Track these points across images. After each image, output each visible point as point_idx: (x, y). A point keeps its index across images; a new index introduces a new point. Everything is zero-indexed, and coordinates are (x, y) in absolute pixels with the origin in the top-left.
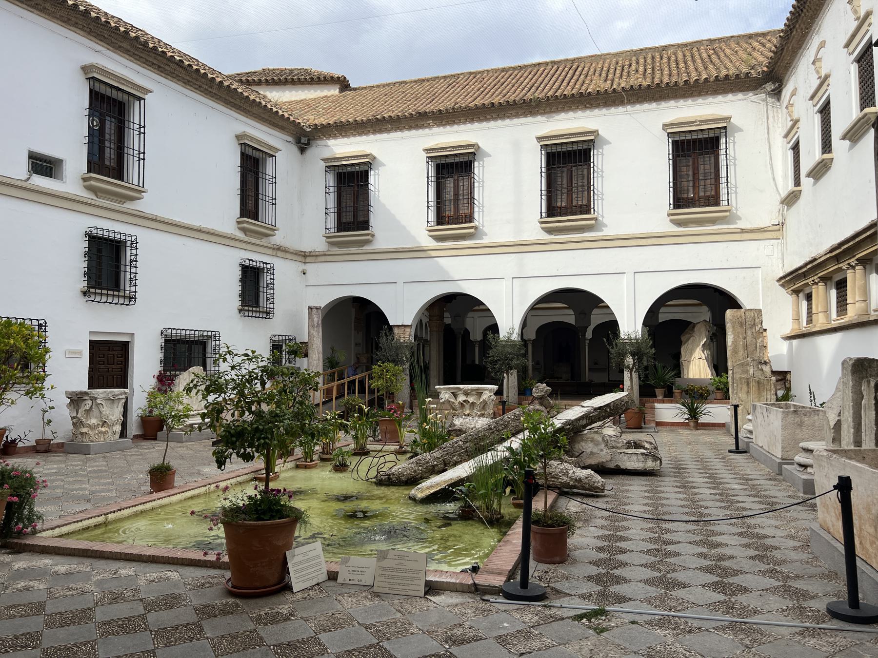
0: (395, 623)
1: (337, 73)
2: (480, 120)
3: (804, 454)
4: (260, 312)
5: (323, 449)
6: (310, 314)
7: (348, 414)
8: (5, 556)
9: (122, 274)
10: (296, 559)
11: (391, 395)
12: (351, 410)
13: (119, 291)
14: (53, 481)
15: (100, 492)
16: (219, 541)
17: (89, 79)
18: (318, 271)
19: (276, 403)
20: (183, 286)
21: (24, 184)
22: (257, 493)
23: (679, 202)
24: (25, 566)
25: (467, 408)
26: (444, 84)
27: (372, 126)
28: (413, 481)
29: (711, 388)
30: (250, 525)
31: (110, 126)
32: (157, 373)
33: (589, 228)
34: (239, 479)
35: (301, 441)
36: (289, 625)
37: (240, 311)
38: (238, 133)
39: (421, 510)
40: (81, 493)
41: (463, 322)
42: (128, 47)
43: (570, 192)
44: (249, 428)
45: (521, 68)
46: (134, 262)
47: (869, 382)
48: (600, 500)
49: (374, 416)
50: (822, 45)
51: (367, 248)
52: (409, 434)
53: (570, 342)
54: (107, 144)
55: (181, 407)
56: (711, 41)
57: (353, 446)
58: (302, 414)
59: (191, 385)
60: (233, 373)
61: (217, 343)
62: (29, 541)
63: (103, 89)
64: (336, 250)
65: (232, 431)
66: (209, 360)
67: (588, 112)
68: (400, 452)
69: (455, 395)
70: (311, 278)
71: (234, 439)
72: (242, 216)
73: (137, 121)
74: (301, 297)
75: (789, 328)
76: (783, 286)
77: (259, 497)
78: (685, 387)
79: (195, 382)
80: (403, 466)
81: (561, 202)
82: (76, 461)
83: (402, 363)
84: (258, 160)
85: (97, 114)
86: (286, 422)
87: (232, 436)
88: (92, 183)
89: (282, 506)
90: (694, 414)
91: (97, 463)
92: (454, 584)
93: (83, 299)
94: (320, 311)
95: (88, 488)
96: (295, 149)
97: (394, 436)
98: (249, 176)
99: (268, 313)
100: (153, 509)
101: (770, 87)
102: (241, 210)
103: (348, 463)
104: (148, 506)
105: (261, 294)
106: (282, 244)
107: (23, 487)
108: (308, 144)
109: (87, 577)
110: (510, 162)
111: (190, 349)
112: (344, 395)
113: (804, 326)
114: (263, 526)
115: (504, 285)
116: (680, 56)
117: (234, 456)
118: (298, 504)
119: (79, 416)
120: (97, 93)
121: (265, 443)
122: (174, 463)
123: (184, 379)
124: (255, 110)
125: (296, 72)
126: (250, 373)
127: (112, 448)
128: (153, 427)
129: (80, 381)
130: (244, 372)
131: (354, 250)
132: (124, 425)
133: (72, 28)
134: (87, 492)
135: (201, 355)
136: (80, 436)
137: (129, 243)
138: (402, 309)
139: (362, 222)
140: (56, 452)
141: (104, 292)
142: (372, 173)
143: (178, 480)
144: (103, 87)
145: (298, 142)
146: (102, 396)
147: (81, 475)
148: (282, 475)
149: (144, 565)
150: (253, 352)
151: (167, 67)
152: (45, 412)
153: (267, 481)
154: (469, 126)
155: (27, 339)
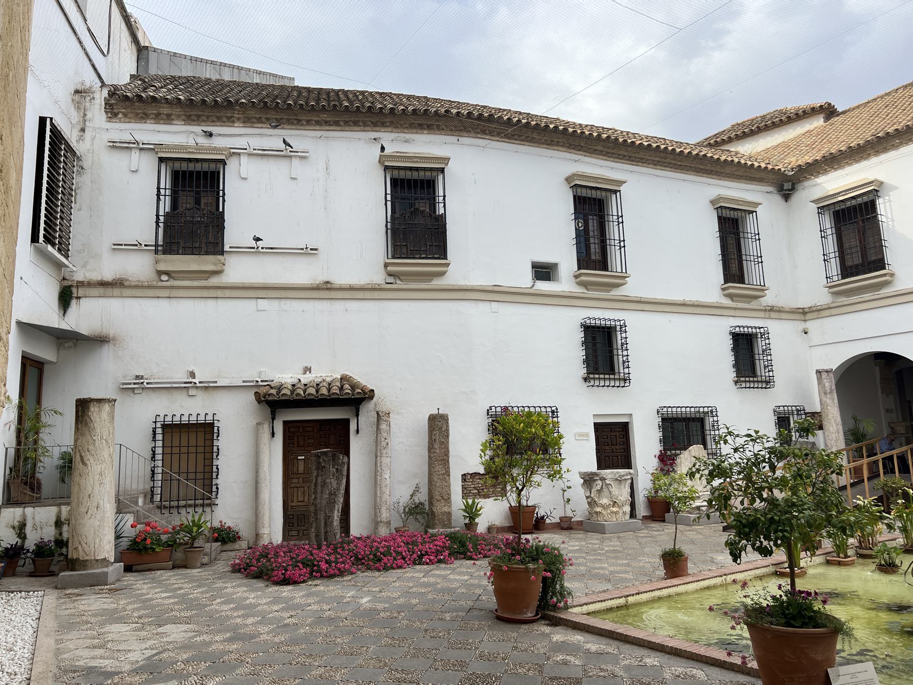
1: (818, 102)
4: (758, 382)
5: (860, 542)
6: (819, 379)
7: (888, 499)
8: (545, 627)
9: (615, 357)
12: (892, 494)
13: (614, 374)
14: (577, 558)
15: (618, 572)
16: (745, 642)
19: (790, 489)
20: (677, 362)
22: (782, 593)
24: (561, 640)
27: (872, 148)
30: (779, 631)
31: (593, 224)
32: (658, 453)
34: (758, 572)
35: (828, 532)
37: (736, 382)
38: (713, 197)
40: (602, 572)
42: (602, 149)
44: (763, 519)
51: (885, 291)
54: (592, 240)
55: (685, 489)
57: (901, 541)
58: (826, 502)
59: (694, 470)
60: (737, 455)
61: (715, 419)
64: (843, 300)
65: (744, 521)
66: (708, 437)
71: (747, 530)
72: (726, 281)
73: (615, 213)
77: (784, 598)
79: (697, 466)
82: (594, 539)
84: (737, 220)
85: (581, 216)
86: (807, 512)
87: (745, 526)
89: (814, 612)
91: (612, 543)
93: (585, 385)
94: (831, 375)
95: (607, 567)
96: (777, 199)
98: (729, 239)
99: (767, 382)
100: (669, 596)
102: (725, 275)
103: (898, 562)
104: (665, 592)
105: (757, 362)
106: (774, 304)
107: (554, 563)
108: (793, 189)
109: (615, 660)
111: (687, 427)
112: (879, 475)
117: (749, 548)
118: (836, 610)
120: (580, 197)
121: (784, 536)
122: (685, 548)
123: (686, 460)
124: (728, 170)
125: (769, 117)
126: (755, 455)
127: (622, 528)
128: (660, 509)
129: (590, 464)
130: (749, 454)
131: (867, 296)
132: (633, 505)
134: (607, 572)
135: (699, 433)
137: (618, 328)
139: (874, 262)
140: (576, 529)
141: (602, 376)
143: (691, 567)
144: (584, 190)
146: (610, 476)
147: (600, 554)
148: (811, 571)
149: (667, 656)
150: (757, 432)
151: (636, 155)
152: (564, 491)
153: (792, 576)
155: (544, 427)
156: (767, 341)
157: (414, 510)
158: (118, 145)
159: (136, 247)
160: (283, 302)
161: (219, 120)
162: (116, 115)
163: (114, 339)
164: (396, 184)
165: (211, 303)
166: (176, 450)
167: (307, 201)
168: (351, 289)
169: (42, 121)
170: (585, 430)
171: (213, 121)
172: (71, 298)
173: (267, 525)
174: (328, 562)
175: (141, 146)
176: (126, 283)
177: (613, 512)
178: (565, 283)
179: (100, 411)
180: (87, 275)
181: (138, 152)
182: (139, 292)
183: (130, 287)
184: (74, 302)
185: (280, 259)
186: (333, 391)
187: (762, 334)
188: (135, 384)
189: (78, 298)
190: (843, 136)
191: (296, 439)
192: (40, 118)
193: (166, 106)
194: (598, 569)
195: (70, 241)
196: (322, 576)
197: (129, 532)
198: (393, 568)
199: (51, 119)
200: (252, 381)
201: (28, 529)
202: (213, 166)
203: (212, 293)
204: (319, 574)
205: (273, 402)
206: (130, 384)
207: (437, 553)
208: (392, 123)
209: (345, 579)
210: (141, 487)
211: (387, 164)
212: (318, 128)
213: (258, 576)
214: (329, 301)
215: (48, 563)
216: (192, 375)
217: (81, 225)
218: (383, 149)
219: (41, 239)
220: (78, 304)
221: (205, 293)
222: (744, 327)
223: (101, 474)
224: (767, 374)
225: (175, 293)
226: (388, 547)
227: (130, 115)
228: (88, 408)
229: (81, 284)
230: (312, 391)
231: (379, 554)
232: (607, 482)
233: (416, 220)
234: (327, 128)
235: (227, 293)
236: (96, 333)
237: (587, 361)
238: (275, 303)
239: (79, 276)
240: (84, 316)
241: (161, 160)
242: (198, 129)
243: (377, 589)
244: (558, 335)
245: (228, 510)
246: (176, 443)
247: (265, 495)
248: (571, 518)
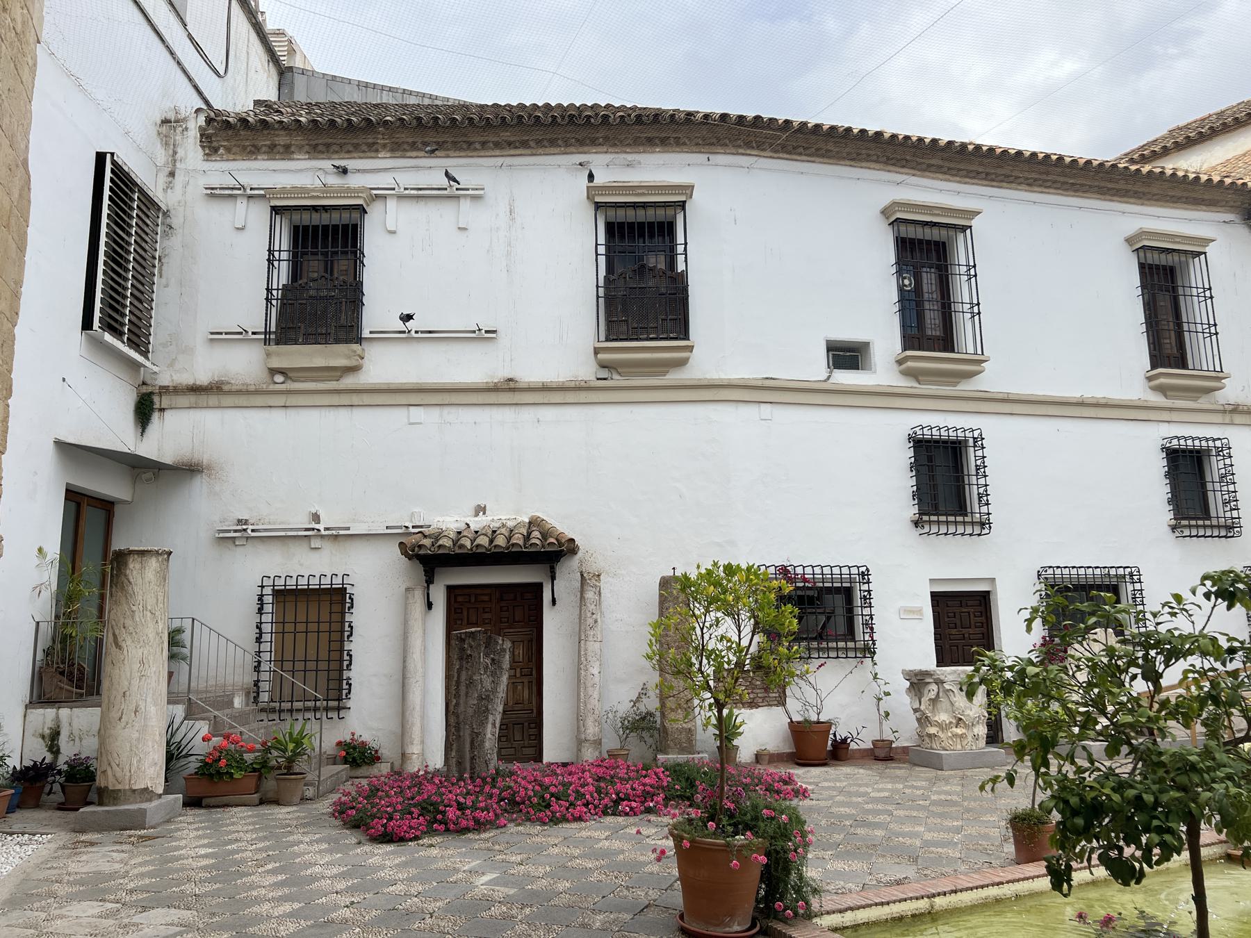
4: (1212, 527)
17: (892, 224)
31: (929, 279)
37: (1174, 528)
40: (909, 842)
42: (940, 163)
46: (981, 469)
61: (1138, 586)
65: (1074, 801)
72: (1154, 366)
73: (963, 261)
82: (917, 781)
88: (910, 364)
91: (950, 787)
93: (915, 532)
95: (920, 833)
99: (1229, 528)
102: (1152, 357)
105: (1210, 494)
119: (922, 708)
120: (1150, 266)
127: (974, 761)
129: (925, 657)
133: (864, 164)
134: (918, 843)
136: (927, 739)
137: (971, 442)
140: (900, 761)
141: (943, 518)
144: (911, 228)
146: (951, 678)
152: (879, 699)
156: (1228, 461)
157: (639, 724)
158: (218, 192)
159: (240, 336)
160: (446, 410)
161: (357, 150)
162: (216, 150)
163: (209, 468)
164: (613, 230)
165: (343, 412)
166: (301, 627)
167: (488, 264)
168: (545, 388)
169: (100, 158)
170: (916, 604)
171: (349, 152)
172: (152, 410)
173: (417, 740)
174: (461, 807)
175: (249, 192)
176: (226, 388)
177: (956, 735)
178: (882, 370)
179: (143, 568)
180: (175, 378)
181: (245, 201)
182: (242, 400)
183: (230, 392)
184: (156, 415)
185: (442, 347)
186: (513, 541)
187: (1219, 451)
188: (236, 531)
189: (162, 410)
191: (465, 613)
192: (98, 153)
193: (282, 132)
194: (904, 835)
195: (152, 330)
196: (447, 830)
197: (199, 748)
198: (567, 821)
199: (112, 154)
200: (400, 527)
201: (63, 741)
202: (346, 217)
203: (345, 399)
204: (443, 826)
205: (430, 558)
206: (229, 531)
207: (647, 796)
208: (606, 139)
209: (483, 836)
210: (239, 680)
211: (598, 199)
212: (498, 152)
213: (355, 825)
214: (513, 408)
215: (60, 789)
216: (316, 518)
217: (166, 311)
218: (591, 177)
219: (96, 324)
220: (162, 418)
221: (335, 399)
222: (1186, 439)
223: (142, 662)
224: (1228, 514)
225: (293, 400)
226: (566, 785)
227: (234, 150)
228: (126, 564)
229: (165, 390)
230: (483, 541)
231: (547, 796)
232: (947, 686)
233: (643, 282)
234: (512, 152)
235: (367, 399)
236: (185, 459)
238: (435, 412)
239: (165, 379)
240: (168, 438)
241: (276, 210)
242: (327, 164)
243: (519, 858)
244: (874, 451)
245: (366, 716)
246: (290, 617)
247: (415, 697)
248: (892, 742)
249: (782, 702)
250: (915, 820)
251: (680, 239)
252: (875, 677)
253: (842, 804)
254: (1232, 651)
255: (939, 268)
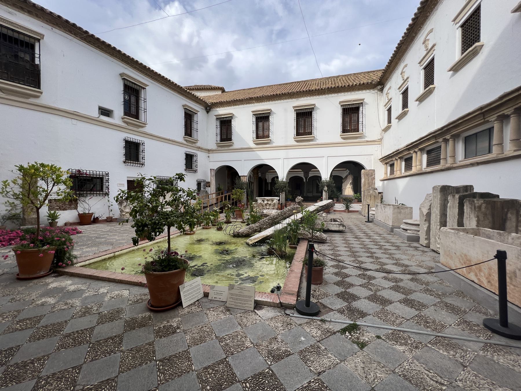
0: (237, 336)
1: (220, 86)
2: (272, 101)
3: (404, 224)
10: (185, 289)
11: (240, 201)
18: (215, 156)
20: (162, 161)
21: (97, 119)
23: (344, 131)
25: (268, 206)
26: (259, 89)
28: (248, 235)
29: (353, 198)
31: (133, 99)
33: (312, 140)
36: (175, 338)
39: (251, 249)
40: (111, 240)
41: (265, 176)
43: (305, 128)
45: (286, 84)
47: (454, 196)
48: (325, 244)
49: (233, 209)
50: (406, 66)
51: (231, 148)
52: (246, 215)
53: (304, 183)
56: (355, 74)
57: (225, 220)
62: (67, 270)
63: (128, 84)
64: (220, 148)
65: (140, 224)
67: (312, 97)
68: (243, 222)
69: (263, 201)
70: (211, 159)
73: (143, 97)
74: (207, 165)
75: (383, 177)
76: (381, 161)
78: (344, 198)
80: (243, 228)
81: (301, 131)
83: (244, 189)
90: (347, 207)
92: (270, 302)
93: (124, 164)
96: (205, 112)
97: (241, 216)
101: (379, 87)
108: (210, 110)
110: (283, 117)
113: (389, 176)
114: (165, 275)
115: (281, 161)
116: (344, 79)
131: (226, 148)
138: (244, 170)
142: (233, 120)
145: (206, 109)
148: (197, 232)
150: (155, 178)
154: (268, 103)
190: (225, 98)
237: (126, 155)
249: (76, 208)
250: (115, 235)
251: (37, 51)
252: (109, 201)
253: (93, 234)
254: (180, 190)
255: (136, 96)
